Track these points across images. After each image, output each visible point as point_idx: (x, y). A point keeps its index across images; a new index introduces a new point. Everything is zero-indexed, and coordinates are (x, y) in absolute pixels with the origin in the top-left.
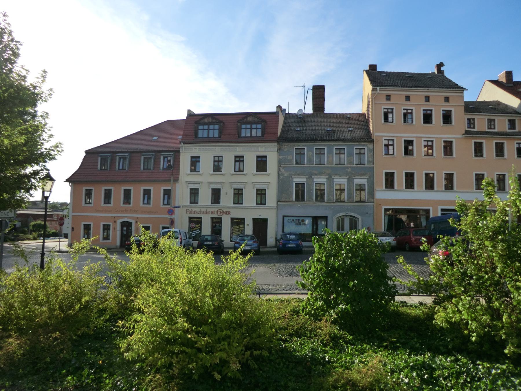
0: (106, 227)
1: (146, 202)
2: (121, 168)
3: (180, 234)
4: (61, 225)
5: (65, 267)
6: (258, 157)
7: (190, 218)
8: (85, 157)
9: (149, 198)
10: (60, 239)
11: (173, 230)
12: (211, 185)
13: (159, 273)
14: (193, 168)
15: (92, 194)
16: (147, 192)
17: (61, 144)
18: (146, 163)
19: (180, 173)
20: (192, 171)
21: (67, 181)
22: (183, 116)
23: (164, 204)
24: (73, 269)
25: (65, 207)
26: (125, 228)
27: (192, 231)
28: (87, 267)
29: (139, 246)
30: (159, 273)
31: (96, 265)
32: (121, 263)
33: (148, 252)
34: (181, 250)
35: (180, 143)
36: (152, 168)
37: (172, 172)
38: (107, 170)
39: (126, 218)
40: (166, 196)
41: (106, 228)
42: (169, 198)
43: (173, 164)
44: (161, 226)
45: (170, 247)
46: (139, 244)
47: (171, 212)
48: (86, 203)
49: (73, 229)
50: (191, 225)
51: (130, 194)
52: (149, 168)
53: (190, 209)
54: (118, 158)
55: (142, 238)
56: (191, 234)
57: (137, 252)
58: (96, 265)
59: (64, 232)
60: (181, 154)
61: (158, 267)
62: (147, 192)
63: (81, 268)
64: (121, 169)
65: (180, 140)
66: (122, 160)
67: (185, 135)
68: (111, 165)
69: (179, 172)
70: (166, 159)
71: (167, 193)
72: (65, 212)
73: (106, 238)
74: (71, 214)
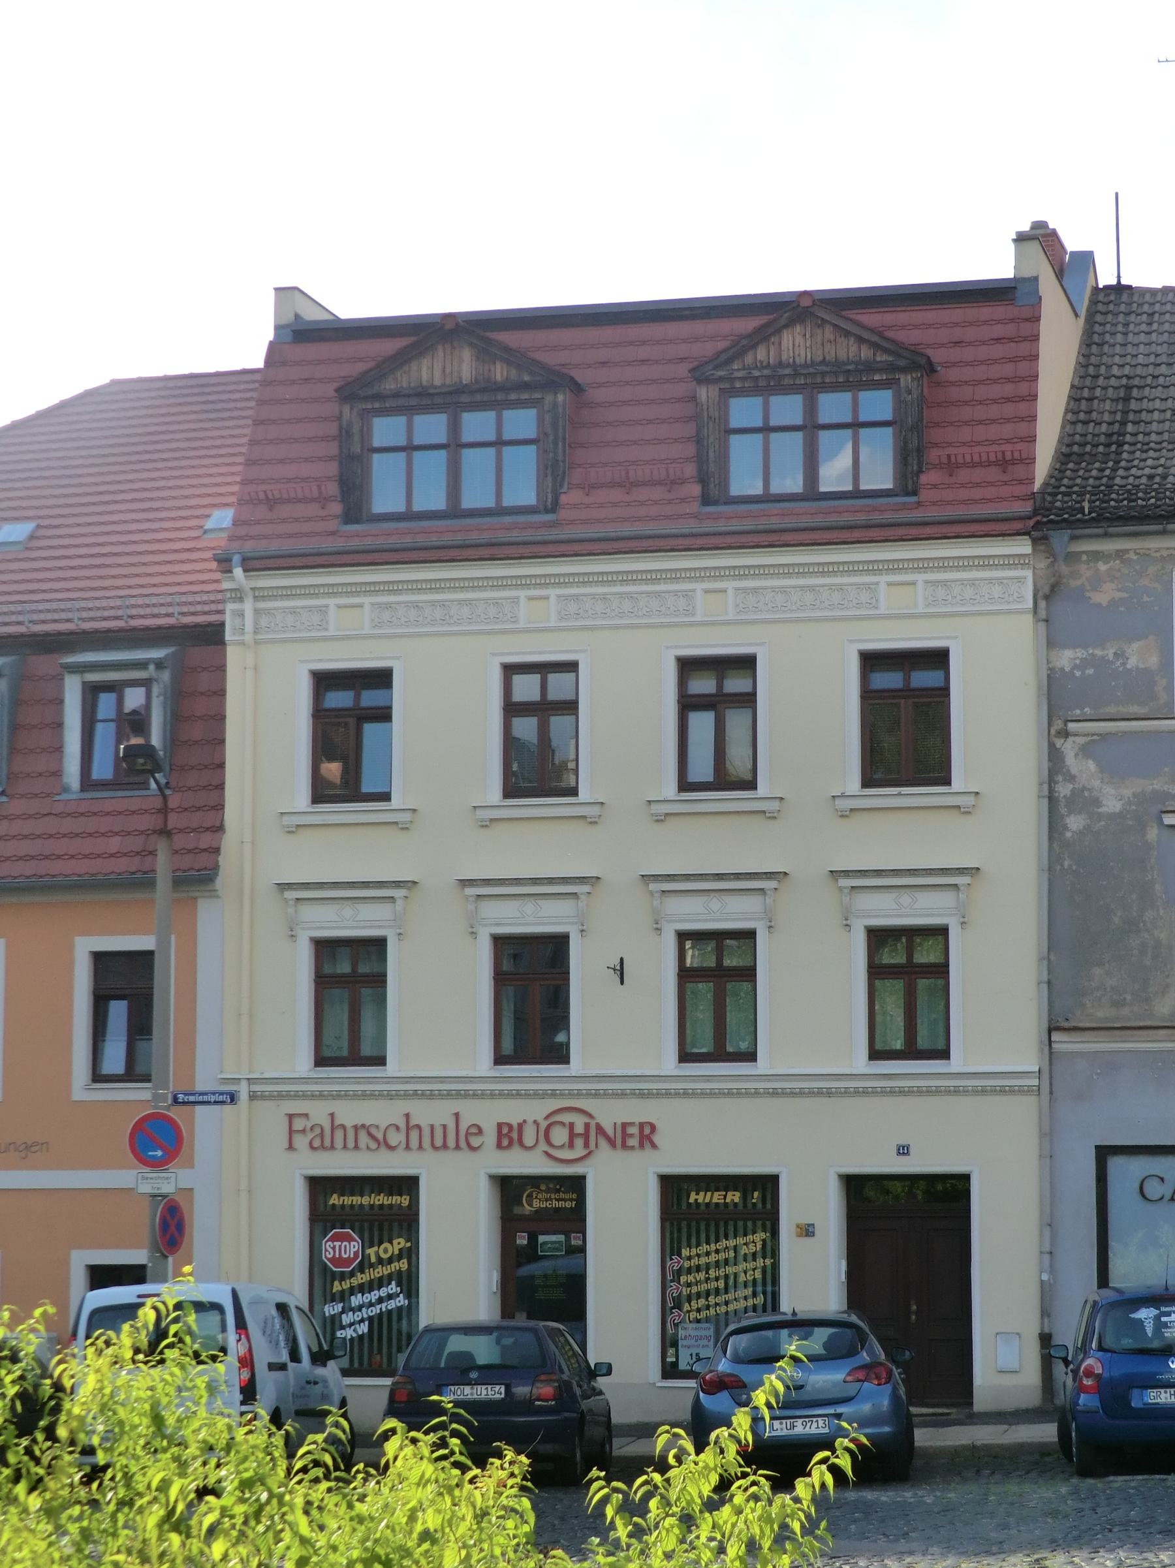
3: (241, 1325)
7: (319, 1186)
14: (333, 770)
20: (321, 793)
23: (98, 1077)
27: (343, 1297)
35: (224, 563)
37: (164, 811)
40: (118, 1011)
42: (141, 1027)
43: (173, 739)
44: (80, 1260)
45: (157, 1420)
47: (158, 1140)
50: (330, 1249)
53: (319, 1113)
56: (334, 1323)
60: (233, 656)
65: (219, 541)
67: (260, 501)
71: (126, 984)
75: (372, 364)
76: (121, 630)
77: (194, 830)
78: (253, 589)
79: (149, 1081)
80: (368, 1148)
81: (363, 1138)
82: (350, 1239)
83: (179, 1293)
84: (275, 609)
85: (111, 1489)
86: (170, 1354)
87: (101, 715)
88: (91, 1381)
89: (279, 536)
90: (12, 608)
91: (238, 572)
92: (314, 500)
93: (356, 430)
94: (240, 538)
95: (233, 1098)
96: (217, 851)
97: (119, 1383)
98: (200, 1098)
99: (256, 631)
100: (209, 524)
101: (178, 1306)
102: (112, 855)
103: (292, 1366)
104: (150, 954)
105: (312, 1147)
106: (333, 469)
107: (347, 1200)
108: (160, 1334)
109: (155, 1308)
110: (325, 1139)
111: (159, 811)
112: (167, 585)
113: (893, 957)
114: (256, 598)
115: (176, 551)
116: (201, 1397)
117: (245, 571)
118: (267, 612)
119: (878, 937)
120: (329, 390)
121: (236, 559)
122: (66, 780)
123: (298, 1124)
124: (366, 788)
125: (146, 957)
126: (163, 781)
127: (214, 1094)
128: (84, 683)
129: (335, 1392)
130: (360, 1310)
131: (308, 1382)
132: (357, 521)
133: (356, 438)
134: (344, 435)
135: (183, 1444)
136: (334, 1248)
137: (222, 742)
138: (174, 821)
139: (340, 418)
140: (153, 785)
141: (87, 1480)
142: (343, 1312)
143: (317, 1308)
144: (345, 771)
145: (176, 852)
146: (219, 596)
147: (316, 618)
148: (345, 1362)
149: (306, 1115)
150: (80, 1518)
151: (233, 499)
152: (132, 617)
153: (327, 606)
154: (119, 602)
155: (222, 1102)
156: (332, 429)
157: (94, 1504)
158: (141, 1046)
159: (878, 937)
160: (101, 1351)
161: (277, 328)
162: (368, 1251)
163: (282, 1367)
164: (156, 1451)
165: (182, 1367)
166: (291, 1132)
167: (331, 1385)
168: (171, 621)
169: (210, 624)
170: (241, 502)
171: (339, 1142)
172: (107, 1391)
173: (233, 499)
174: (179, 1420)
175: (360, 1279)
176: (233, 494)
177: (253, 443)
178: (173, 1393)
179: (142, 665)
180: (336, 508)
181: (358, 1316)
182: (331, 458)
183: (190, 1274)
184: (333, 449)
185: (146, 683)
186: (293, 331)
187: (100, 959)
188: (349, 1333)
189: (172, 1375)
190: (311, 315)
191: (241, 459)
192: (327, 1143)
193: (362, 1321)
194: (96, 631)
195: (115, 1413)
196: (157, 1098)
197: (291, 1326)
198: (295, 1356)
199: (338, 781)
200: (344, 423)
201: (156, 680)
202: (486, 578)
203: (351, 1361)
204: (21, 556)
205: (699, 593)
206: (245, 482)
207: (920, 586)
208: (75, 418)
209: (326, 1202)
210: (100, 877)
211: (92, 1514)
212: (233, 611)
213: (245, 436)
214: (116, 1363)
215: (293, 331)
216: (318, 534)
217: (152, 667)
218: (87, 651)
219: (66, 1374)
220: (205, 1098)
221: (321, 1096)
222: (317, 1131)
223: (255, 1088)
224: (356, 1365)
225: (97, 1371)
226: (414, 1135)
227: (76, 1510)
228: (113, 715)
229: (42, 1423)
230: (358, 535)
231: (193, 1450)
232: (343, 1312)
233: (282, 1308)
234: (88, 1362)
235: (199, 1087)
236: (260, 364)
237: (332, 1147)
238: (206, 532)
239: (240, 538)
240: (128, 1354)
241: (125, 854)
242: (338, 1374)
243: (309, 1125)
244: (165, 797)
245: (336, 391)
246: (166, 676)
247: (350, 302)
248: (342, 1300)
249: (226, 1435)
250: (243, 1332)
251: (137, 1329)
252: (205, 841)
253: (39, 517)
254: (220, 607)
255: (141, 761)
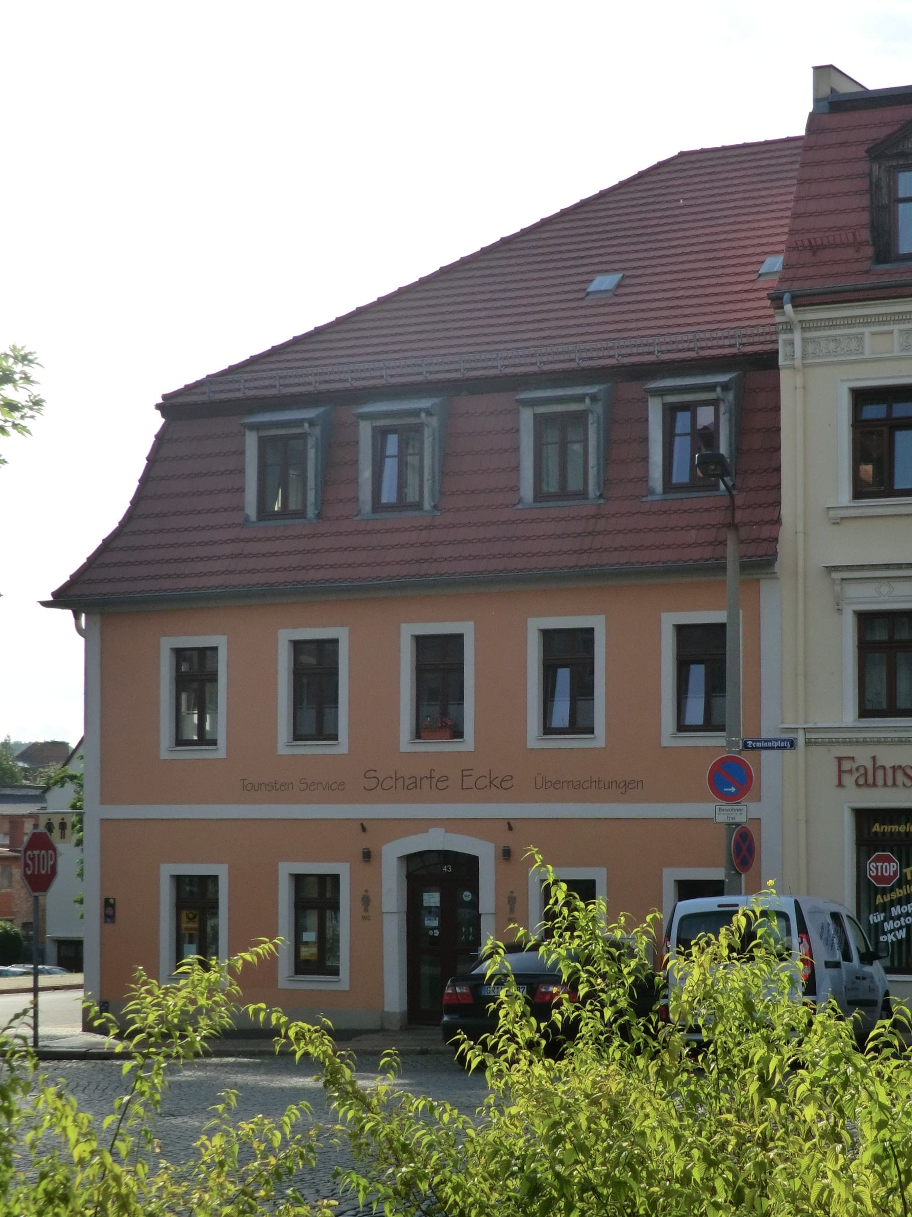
0: (312, 892)
1: (561, 714)
2: (388, 495)
3: (803, 929)
4: (40, 882)
5: (86, 1136)
6: (861, 397)
7: (864, 818)
8: (161, 438)
9: (583, 689)
10: (36, 973)
11: (756, 903)
12: (853, 591)
13: (686, 1178)
14: (867, 470)
15: (213, 677)
16: (568, 653)
17: (24, 359)
18: (552, 454)
19: (786, 510)
20: (860, 491)
21: (60, 599)
22: (785, 114)
23: (682, 727)
24: (135, 1156)
25: (53, 770)
26: (432, 899)
27: (885, 908)
28: (217, 1140)
29: (540, 1008)
30: (686, 1178)
31: (279, 1130)
32: (428, 1116)
33: (602, 1045)
34: (828, 1033)
35: (777, 301)
36: (311, 512)
37: (732, 507)
38: (301, 514)
39: (440, 825)
40: (698, 673)
41: (316, 898)
42: (716, 685)
43: (737, 449)
44: (671, 875)
45: (749, 1006)
46: (537, 987)
47: (732, 778)
48: (180, 741)
49: (109, 909)
50: (873, 868)
51: (459, 669)
52: (574, 484)
53: (863, 756)
54: (365, 430)
55: (556, 954)
56: (878, 929)
57: (531, 1045)
58: (279, 1130)
59: (57, 928)
60: (785, 378)
61: (678, 1139)
62: (568, 653)
63: (180, 1148)
64: (390, 507)
65: (772, 282)
66: (392, 444)
67: (804, 248)
68: (324, 483)
69: (777, 504)
70: (683, 421)
71: (705, 652)
72: (59, 801)
73: (317, 962)
74: (95, 812)
75: (896, 128)
76: (693, 359)
77: (756, 524)
78: (800, 321)
79: (724, 730)
80: (904, 785)
81: (900, 777)
82: (890, 860)
83: (763, 903)
84: (839, 336)
85: (713, 1061)
86: (757, 953)
87: (678, 430)
88: (696, 973)
89: (822, 276)
90: (605, 344)
91: (788, 308)
92: (849, 245)
93: (884, 184)
94: (788, 280)
95: (792, 744)
96: (776, 540)
97: (718, 975)
98: (766, 745)
99: (804, 357)
100: (763, 269)
101: (764, 913)
102: (689, 546)
103: (843, 963)
104: (723, 626)
105: (858, 785)
106: (865, 217)
107: (887, 828)
108: (749, 936)
109: (745, 915)
110: (868, 778)
111: (727, 508)
112: (729, 321)
113: (880, 635)
114: (804, 329)
115: (736, 292)
116: (785, 988)
117: (794, 307)
118: (813, 340)
119: (865, 619)
120: (861, 151)
121: (787, 297)
122: (651, 484)
123: (846, 766)
124: (899, 485)
125: (719, 629)
126: (730, 483)
127: (777, 741)
128: (664, 405)
129: (880, 987)
130: (899, 919)
131: (858, 978)
132: (885, 261)
133: (884, 191)
134: (874, 189)
135: (770, 1026)
136: (877, 868)
137: (778, 449)
138: (739, 516)
139: (870, 174)
140: (722, 487)
141: (693, 1054)
142: (885, 920)
143: (862, 916)
144: (877, 472)
145: (742, 542)
146: (773, 329)
147: (853, 345)
148: (887, 962)
149: (853, 758)
150: (687, 1083)
151: (783, 247)
152: (702, 348)
153: (862, 334)
154: (691, 337)
155: (785, 748)
156: (864, 184)
157: (700, 1072)
158: (581, 704)
159: (865, 619)
160: (703, 950)
161: (816, 101)
162: (905, 871)
163: (837, 965)
164: (748, 1031)
165: (768, 963)
166: (840, 772)
167: (876, 979)
168: (734, 350)
169: (766, 352)
170: (790, 249)
171: (880, 781)
172: (709, 982)
173: (783, 247)
174: (767, 1007)
175: (899, 893)
176: (782, 242)
177: (798, 199)
178: (760, 984)
179: (711, 388)
180: (869, 251)
181: (897, 924)
182: (863, 209)
183: (772, 887)
184: (865, 201)
185: (715, 403)
186: (831, 103)
187: (681, 630)
188: (890, 938)
189: (761, 970)
190: (844, 89)
191: (788, 213)
192: (870, 781)
193: (901, 928)
194: (673, 361)
195: (716, 1000)
196: (730, 744)
197: (843, 931)
198: (847, 957)
199: (871, 480)
200: (874, 180)
201: (723, 400)
202: (829, 319)
203: (892, 961)
204: (611, 302)
205: (867, 336)
206: (792, 233)
207: (896, 333)
208: (651, 186)
209: (870, 829)
210: (670, 564)
211: (698, 1081)
212: (784, 341)
213: (791, 193)
214: (715, 959)
215: (831, 103)
216: (854, 273)
217: (719, 389)
218: (666, 378)
219: (676, 967)
220: (770, 744)
221: (865, 742)
222: (862, 771)
223: (809, 736)
224: (904, 965)
225: (701, 966)
226: (880, 774)
227: (685, 1076)
228: (688, 430)
229: (657, 1007)
230: (888, 273)
231: (779, 1031)
232: (885, 920)
233: (836, 917)
234: (693, 958)
235: (764, 736)
236: (801, 132)
237: (874, 785)
238: (588, 294)
239: (788, 280)
240: (725, 952)
241: (700, 545)
242: (882, 971)
243: (855, 766)
244: (732, 497)
245: (867, 151)
246: (731, 396)
247: (876, 76)
248: (884, 911)
249: (805, 1020)
250: (804, 936)
251: (732, 933)
252: (766, 531)
253: (625, 269)
254: (774, 337)
255: (713, 467)
